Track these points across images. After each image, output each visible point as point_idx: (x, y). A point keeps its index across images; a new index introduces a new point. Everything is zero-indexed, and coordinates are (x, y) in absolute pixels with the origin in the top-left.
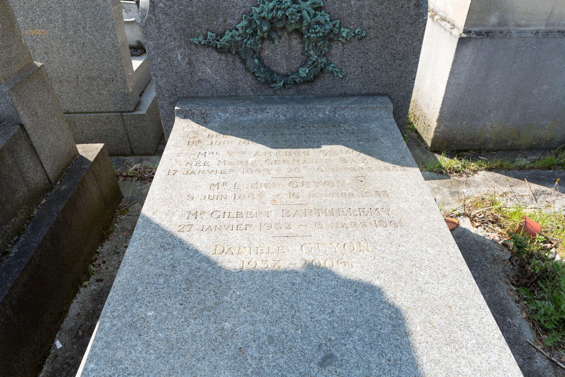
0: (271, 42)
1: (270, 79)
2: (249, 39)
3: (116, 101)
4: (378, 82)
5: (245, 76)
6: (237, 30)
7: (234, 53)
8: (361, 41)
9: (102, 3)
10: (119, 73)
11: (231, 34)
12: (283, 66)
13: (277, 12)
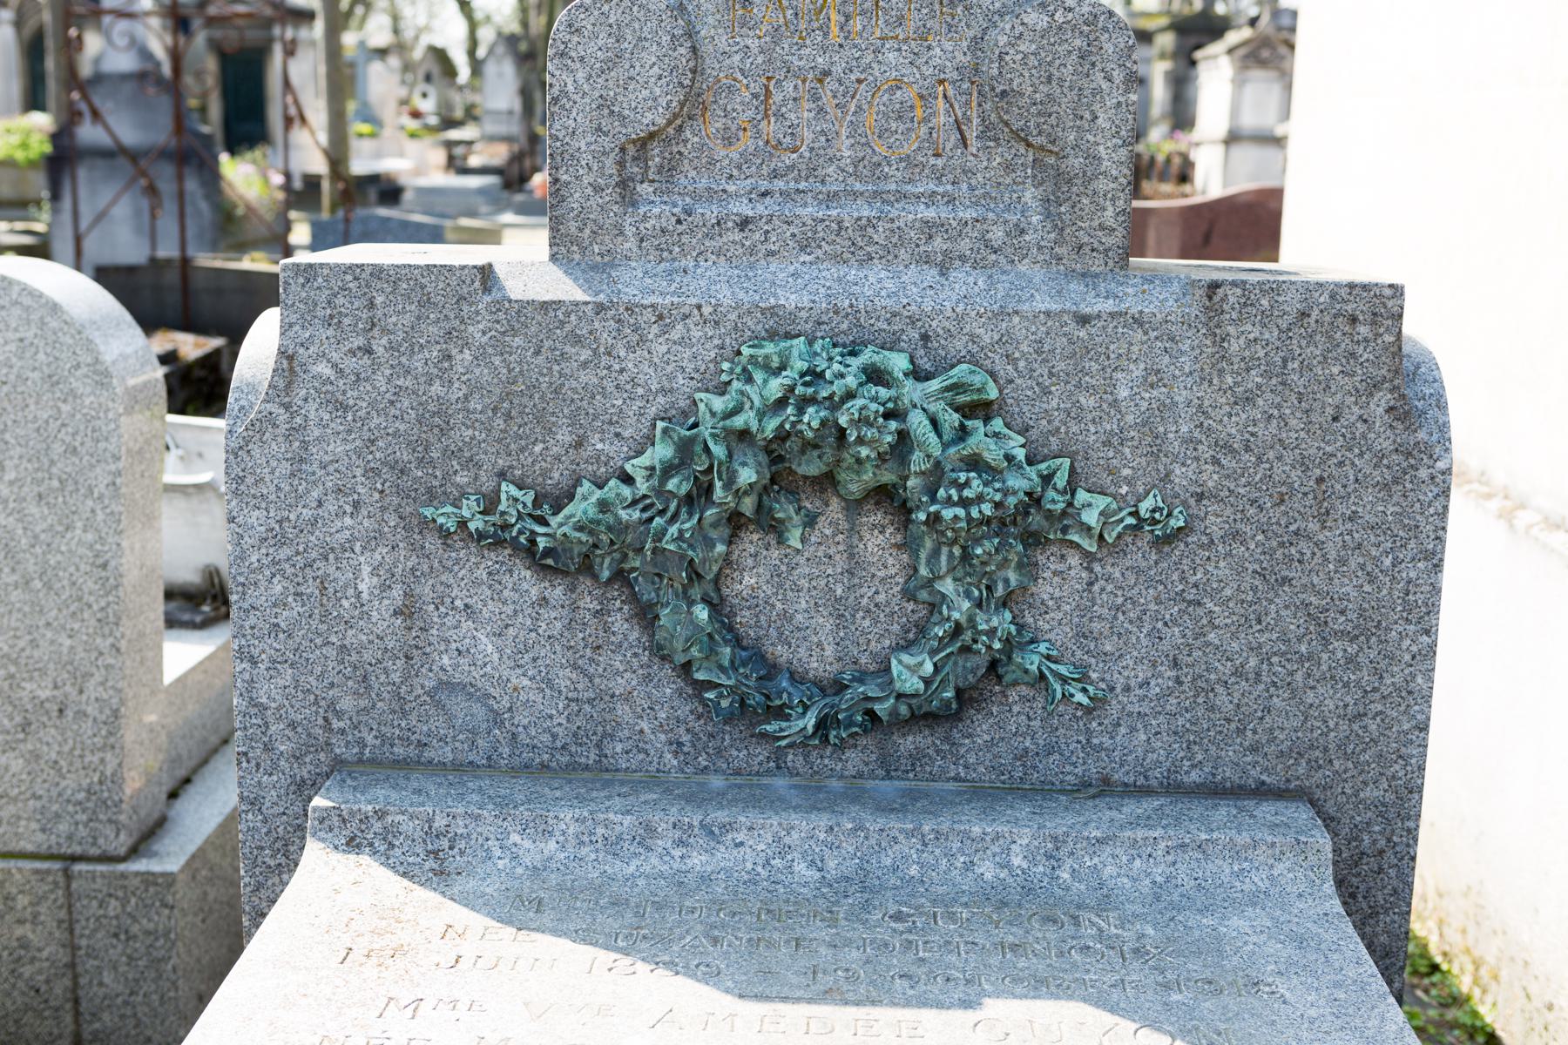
0: (771, 538)
1: (759, 698)
2: (674, 518)
3: (55, 807)
4: (1255, 732)
5: (648, 678)
6: (628, 479)
7: (605, 574)
8: (1166, 549)
9: (88, 390)
10: (98, 678)
11: (598, 494)
12: (819, 644)
13: (801, 411)
